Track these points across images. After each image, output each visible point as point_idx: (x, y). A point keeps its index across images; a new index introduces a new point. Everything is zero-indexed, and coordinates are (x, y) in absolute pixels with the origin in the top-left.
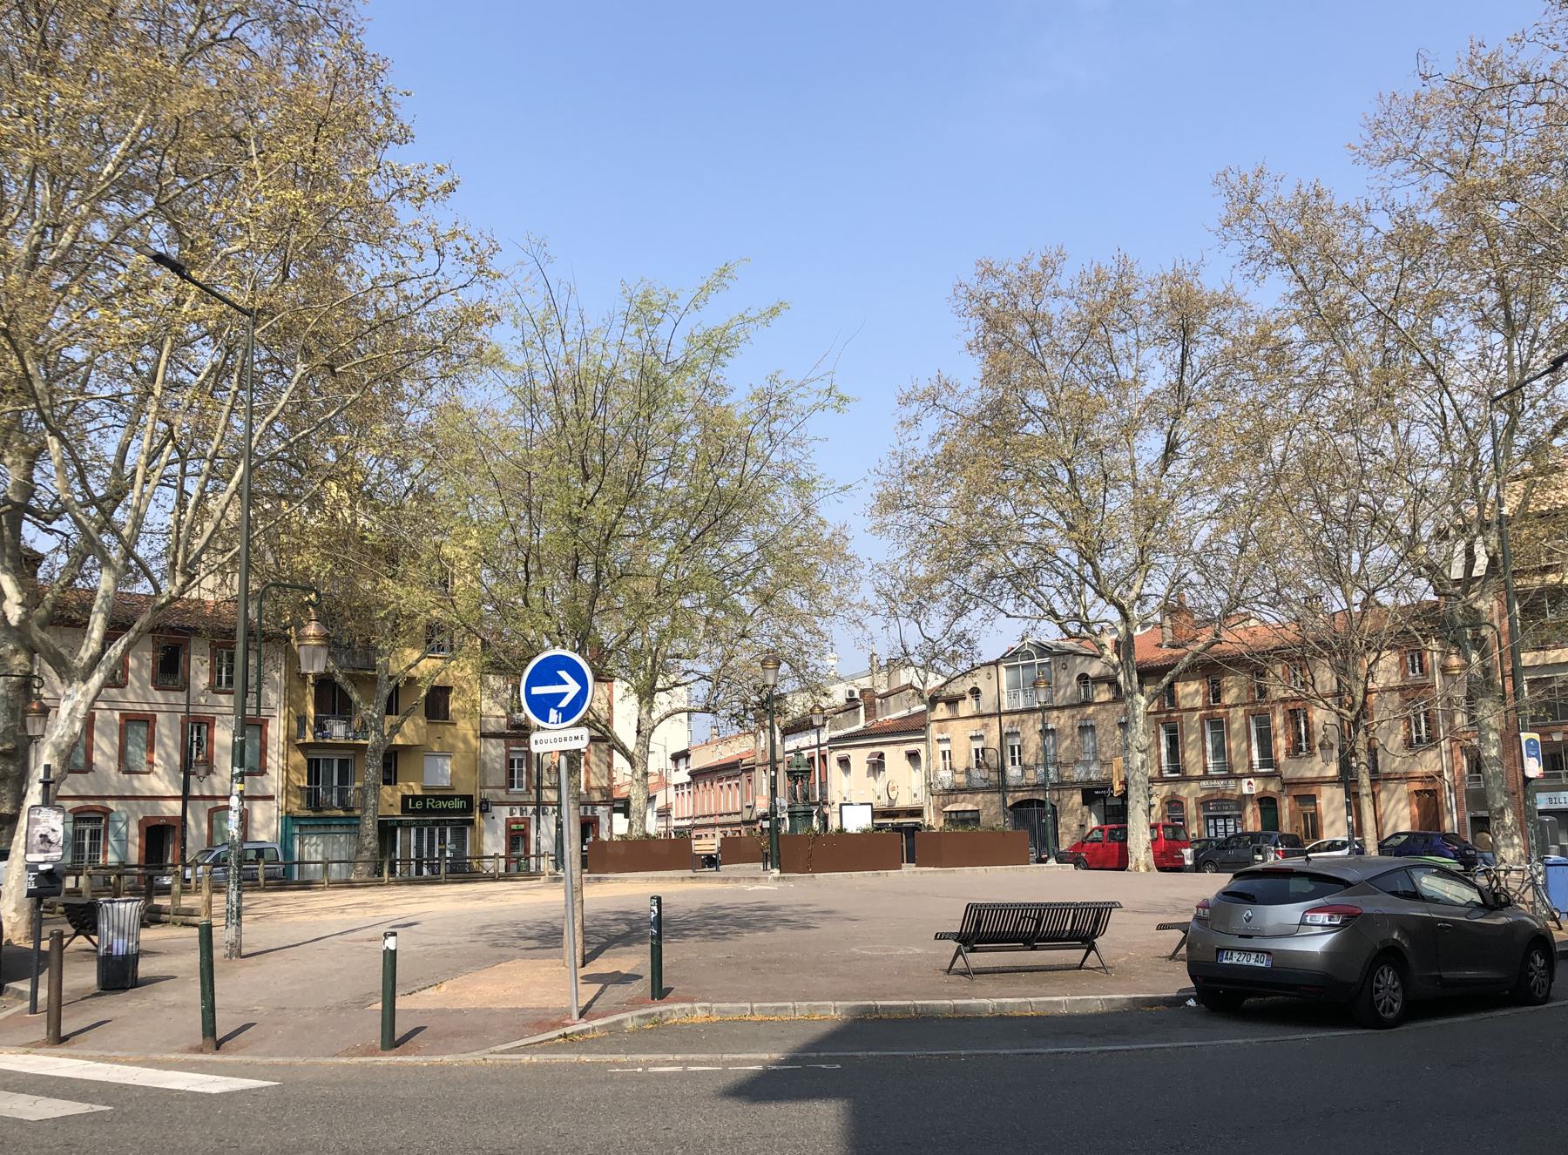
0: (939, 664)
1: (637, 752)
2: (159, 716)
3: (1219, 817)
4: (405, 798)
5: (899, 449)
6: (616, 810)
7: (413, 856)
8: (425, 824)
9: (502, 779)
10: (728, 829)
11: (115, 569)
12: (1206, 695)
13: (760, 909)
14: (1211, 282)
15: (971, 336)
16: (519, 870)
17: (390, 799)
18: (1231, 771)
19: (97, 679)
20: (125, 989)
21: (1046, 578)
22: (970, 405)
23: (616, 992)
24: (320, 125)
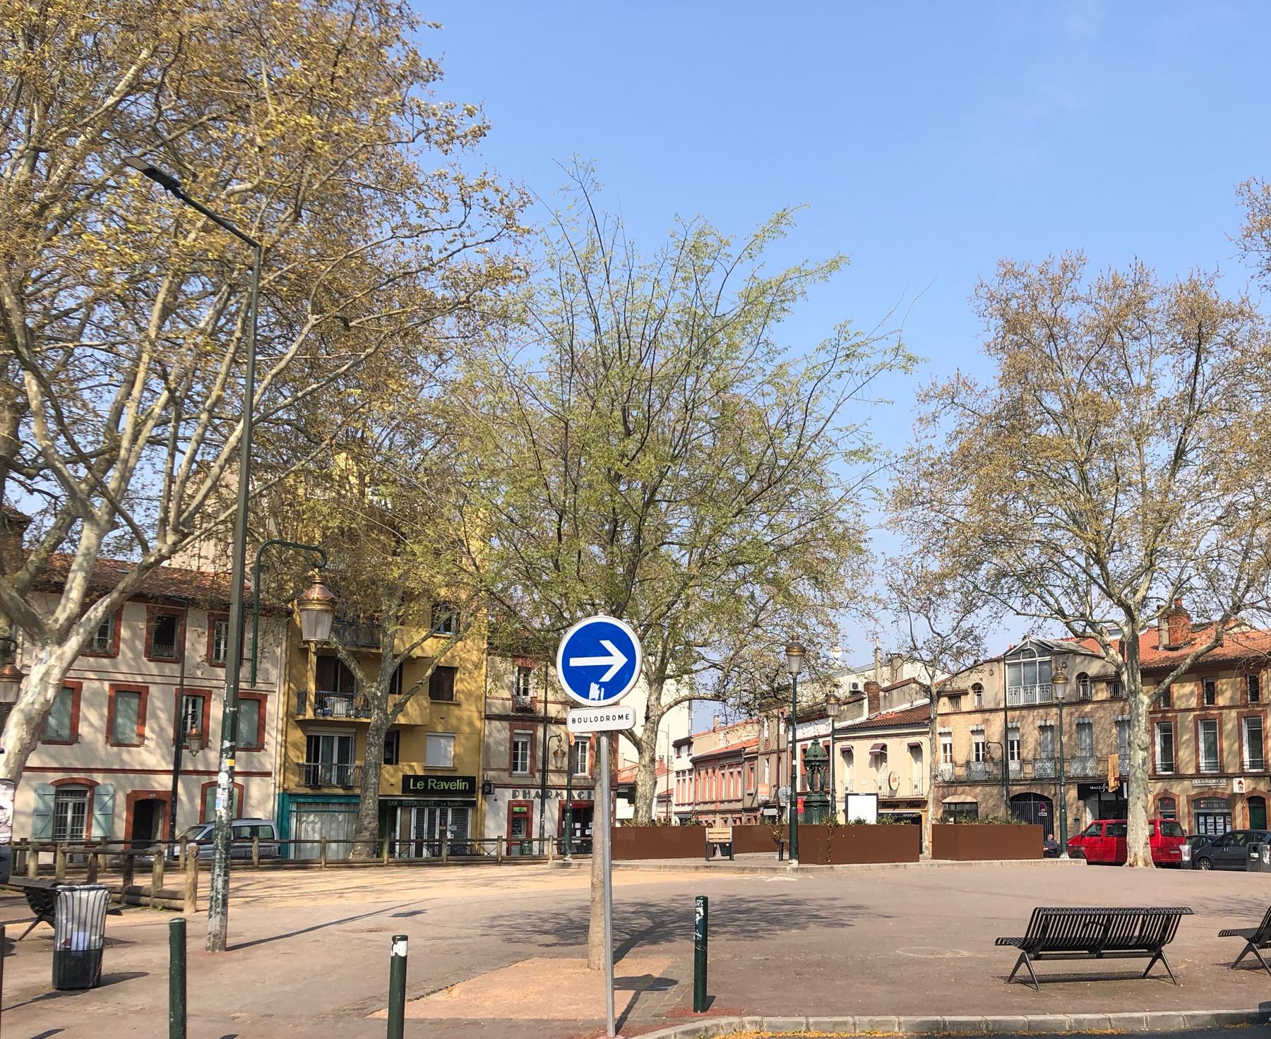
0: (946, 658)
1: (645, 738)
2: (153, 689)
3: (1210, 814)
4: (406, 779)
5: (916, 446)
6: (620, 795)
7: (413, 837)
8: (427, 804)
9: (505, 761)
10: (729, 816)
11: (98, 525)
12: (1200, 697)
13: (785, 903)
14: (1226, 293)
15: (990, 337)
16: (522, 852)
17: (392, 778)
18: (1222, 770)
19: (73, 643)
20: (84, 989)
21: (1054, 578)
22: (987, 405)
23: (653, 1001)
24: (339, 52)
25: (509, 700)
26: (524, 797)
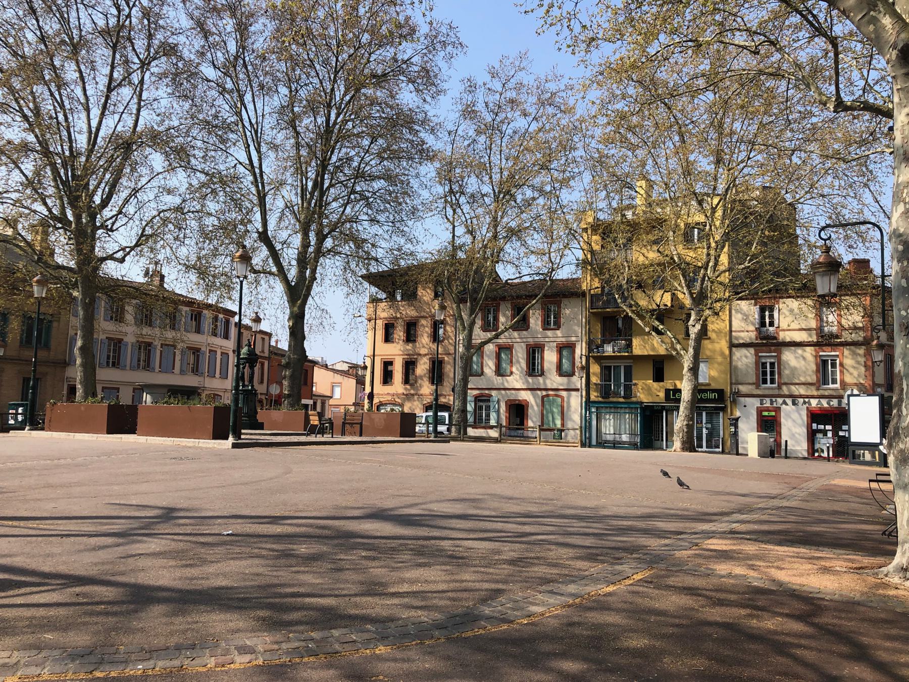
25: (752, 331)
26: (772, 404)
